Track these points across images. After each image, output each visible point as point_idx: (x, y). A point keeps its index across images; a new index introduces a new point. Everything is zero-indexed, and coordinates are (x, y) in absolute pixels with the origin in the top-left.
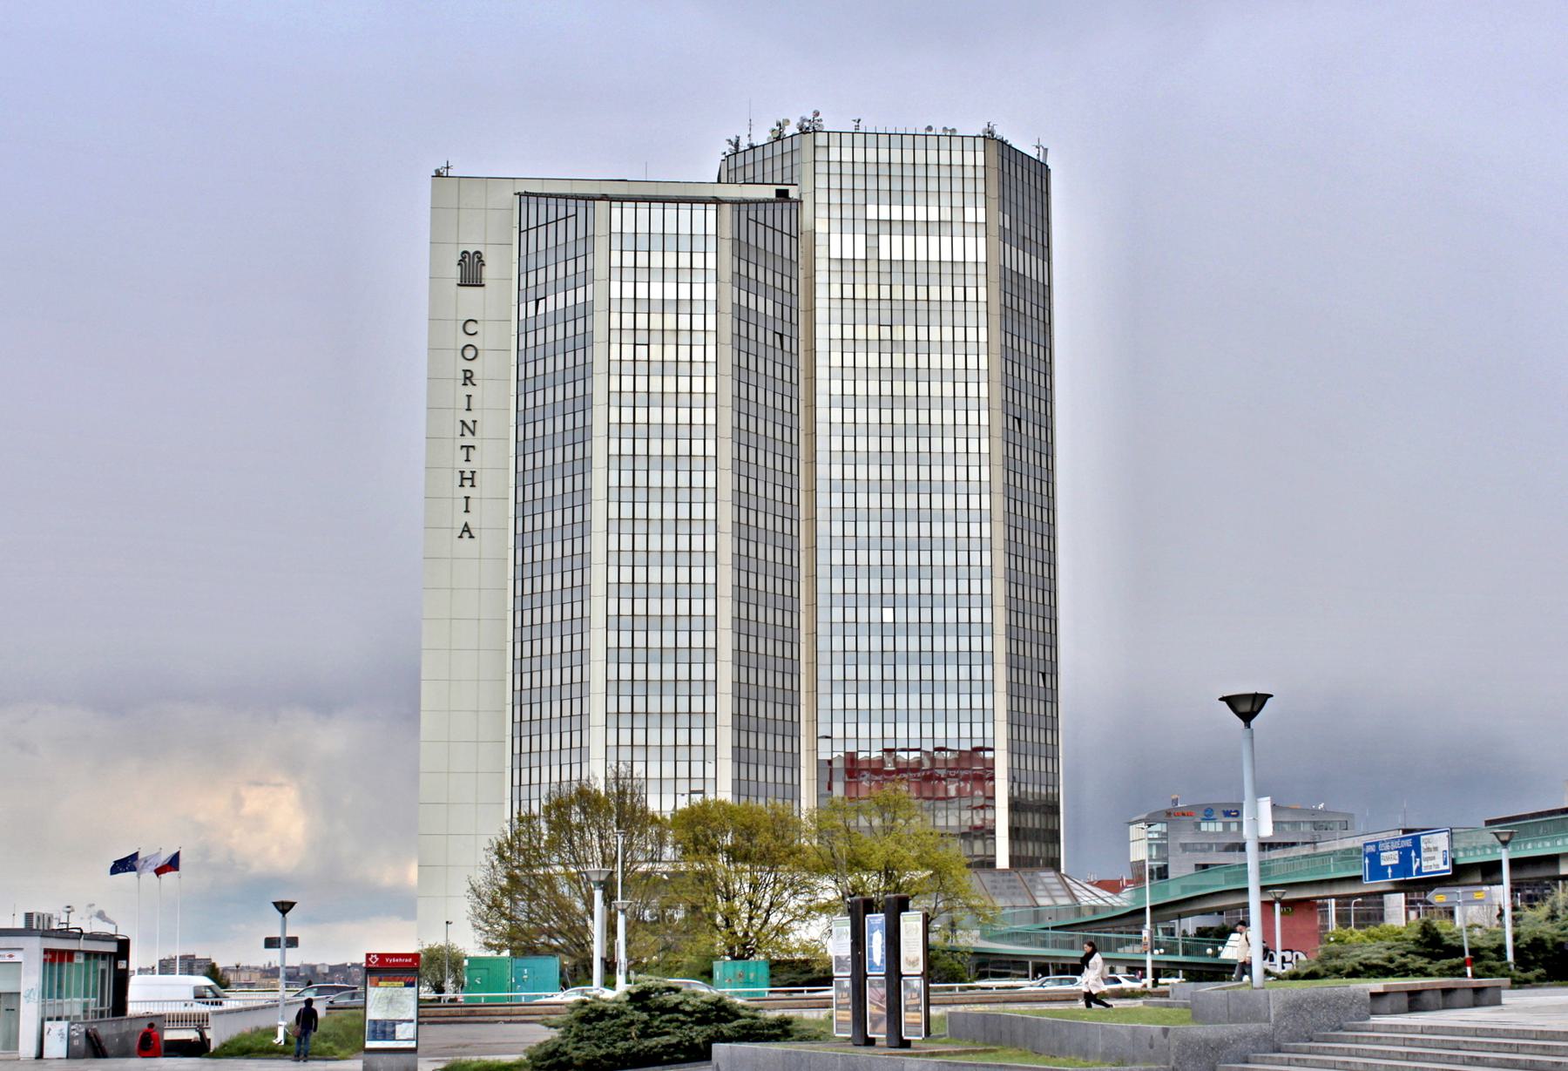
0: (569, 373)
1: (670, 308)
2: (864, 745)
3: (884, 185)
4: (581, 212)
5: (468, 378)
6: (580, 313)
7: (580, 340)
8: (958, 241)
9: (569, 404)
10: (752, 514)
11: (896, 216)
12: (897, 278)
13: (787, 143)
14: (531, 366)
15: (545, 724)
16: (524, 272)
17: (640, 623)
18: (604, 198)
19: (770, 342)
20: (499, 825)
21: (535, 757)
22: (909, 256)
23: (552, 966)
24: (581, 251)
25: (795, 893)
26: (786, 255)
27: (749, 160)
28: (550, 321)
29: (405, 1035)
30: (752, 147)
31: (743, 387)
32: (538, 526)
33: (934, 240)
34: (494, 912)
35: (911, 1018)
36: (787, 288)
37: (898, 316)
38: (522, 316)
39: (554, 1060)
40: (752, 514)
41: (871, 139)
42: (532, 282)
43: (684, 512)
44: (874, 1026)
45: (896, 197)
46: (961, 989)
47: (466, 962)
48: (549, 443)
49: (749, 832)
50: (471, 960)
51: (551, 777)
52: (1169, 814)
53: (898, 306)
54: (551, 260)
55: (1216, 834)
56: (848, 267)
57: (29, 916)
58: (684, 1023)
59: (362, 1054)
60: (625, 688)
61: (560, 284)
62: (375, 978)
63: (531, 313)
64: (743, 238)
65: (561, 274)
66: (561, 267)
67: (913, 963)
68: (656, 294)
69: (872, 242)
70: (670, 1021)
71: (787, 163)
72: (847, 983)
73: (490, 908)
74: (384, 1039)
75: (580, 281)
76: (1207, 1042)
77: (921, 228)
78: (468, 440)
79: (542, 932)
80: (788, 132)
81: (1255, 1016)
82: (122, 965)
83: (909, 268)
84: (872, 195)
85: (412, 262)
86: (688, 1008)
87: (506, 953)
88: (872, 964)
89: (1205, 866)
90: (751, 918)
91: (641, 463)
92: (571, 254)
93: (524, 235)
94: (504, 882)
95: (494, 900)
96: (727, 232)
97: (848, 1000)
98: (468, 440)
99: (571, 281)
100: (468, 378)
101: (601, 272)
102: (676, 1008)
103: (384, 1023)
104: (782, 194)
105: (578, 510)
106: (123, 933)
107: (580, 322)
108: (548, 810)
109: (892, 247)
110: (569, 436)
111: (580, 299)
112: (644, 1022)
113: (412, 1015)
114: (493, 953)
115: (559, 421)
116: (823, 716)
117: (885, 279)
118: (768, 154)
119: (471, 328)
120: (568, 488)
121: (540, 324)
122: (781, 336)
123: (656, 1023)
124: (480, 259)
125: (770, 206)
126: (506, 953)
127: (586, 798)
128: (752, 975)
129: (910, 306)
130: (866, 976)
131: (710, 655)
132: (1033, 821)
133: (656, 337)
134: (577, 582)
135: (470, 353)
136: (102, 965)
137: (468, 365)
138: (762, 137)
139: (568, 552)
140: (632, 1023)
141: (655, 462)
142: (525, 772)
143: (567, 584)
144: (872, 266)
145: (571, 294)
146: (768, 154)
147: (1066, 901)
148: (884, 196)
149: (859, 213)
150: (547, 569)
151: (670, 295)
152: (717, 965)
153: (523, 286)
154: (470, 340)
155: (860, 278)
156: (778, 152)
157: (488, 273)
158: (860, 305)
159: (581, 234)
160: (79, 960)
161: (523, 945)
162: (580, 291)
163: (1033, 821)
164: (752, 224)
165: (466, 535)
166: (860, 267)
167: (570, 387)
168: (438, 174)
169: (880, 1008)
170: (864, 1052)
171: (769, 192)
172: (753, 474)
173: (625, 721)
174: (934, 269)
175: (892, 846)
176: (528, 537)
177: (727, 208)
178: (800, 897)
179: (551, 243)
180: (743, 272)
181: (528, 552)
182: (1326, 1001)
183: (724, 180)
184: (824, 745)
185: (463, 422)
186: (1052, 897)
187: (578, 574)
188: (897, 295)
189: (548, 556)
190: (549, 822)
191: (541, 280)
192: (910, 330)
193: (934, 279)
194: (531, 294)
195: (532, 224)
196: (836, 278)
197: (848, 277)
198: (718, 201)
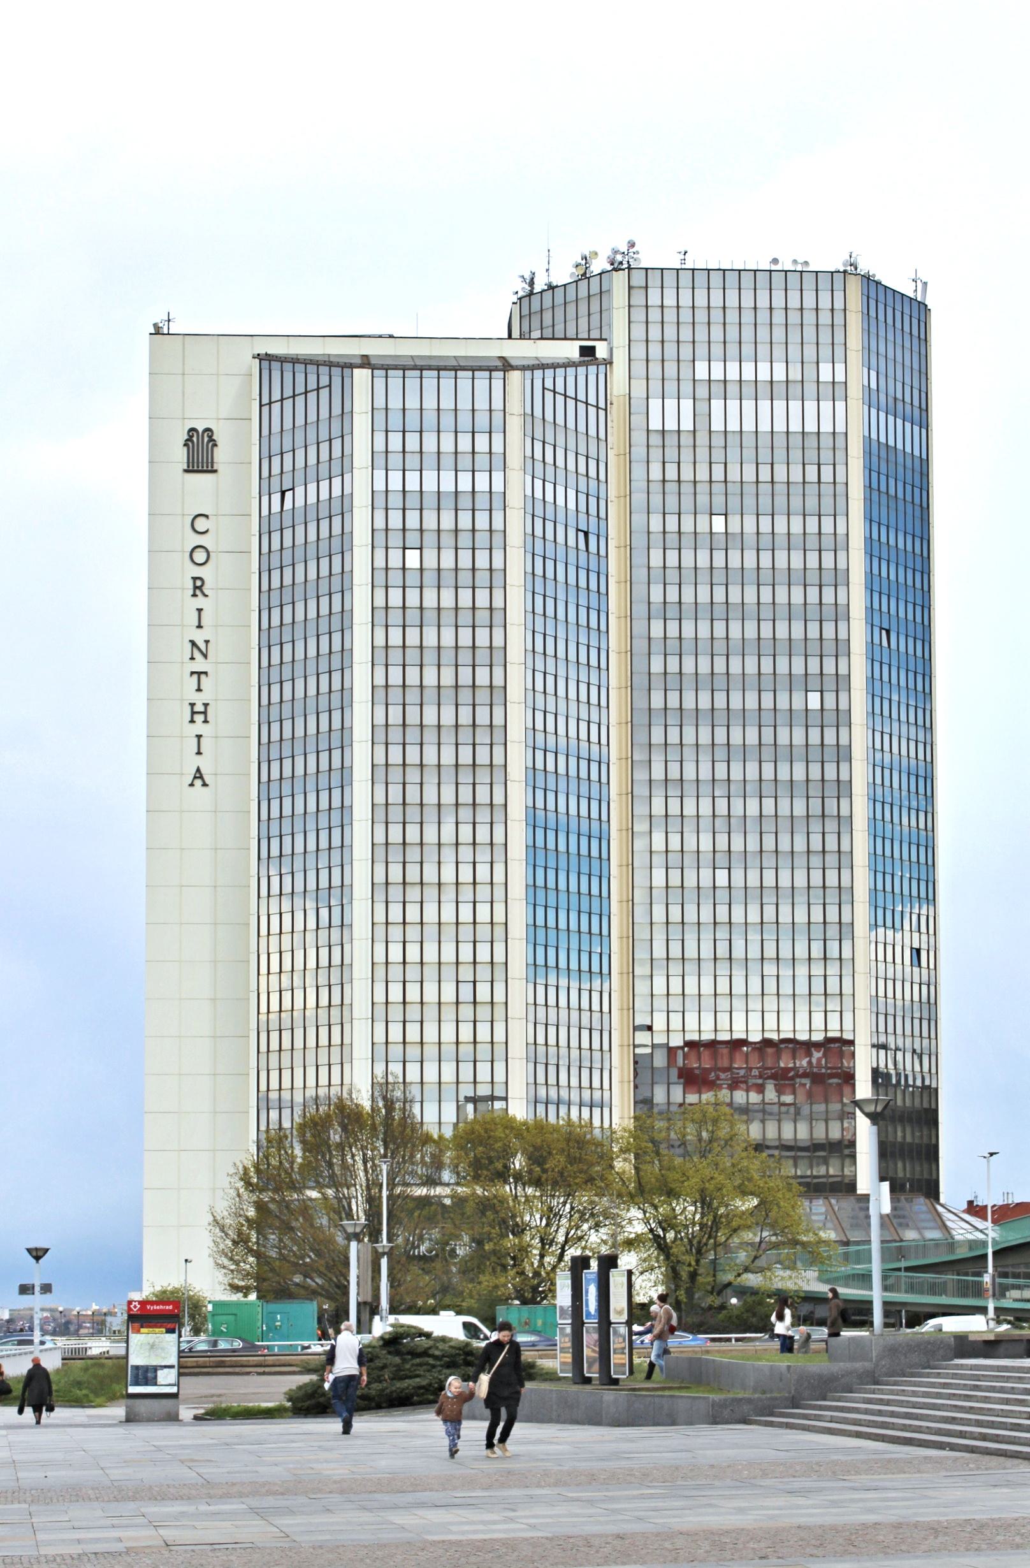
3: (717, 333)
4: (336, 381)
5: (198, 587)
6: (336, 509)
7: (336, 543)
8: (811, 406)
9: (324, 545)
10: (550, 757)
13: (595, 282)
14: (276, 574)
16: (266, 456)
19: (571, 542)
21: (286, 1056)
23: (308, 1311)
24: (336, 432)
25: (597, 1226)
26: (592, 431)
27: (548, 303)
28: (299, 519)
29: (167, 1380)
30: (551, 287)
31: (539, 600)
32: (287, 773)
33: (780, 405)
34: (241, 1248)
35: (618, 1359)
36: (592, 473)
37: (734, 502)
38: (265, 512)
39: (313, 1402)
41: (701, 278)
42: (276, 470)
44: (589, 1367)
46: (737, 1340)
47: (210, 1307)
48: (299, 595)
49: (537, 1157)
50: (216, 1304)
51: (305, 1085)
53: (734, 489)
56: (671, 441)
58: (434, 1366)
59: (124, 1401)
61: (312, 473)
62: (137, 1325)
63: (276, 508)
65: (312, 460)
67: (620, 1313)
68: (430, 486)
69: (702, 407)
70: (420, 1365)
71: (595, 307)
72: (568, 1330)
73: (235, 1243)
74: (146, 1384)
75: (336, 470)
76: (820, 1376)
79: (296, 1268)
80: (599, 265)
81: (865, 1357)
83: (749, 441)
86: (437, 1353)
87: (253, 1297)
88: (589, 1315)
90: (542, 1256)
92: (324, 436)
93: (265, 409)
94: (251, 1213)
95: (240, 1233)
97: (569, 1344)
98: (200, 664)
99: (324, 468)
100: (198, 587)
102: (425, 1353)
103: (146, 1369)
104: (588, 352)
108: (302, 1127)
109: (727, 415)
110: (324, 584)
111: (336, 492)
112: (397, 1365)
113: (173, 1360)
114: (238, 1297)
116: (641, 1004)
118: (571, 295)
119: (201, 524)
120: (324, 727)
121: (287, 522)
122: (586, 534)
123: (408, 1366)
124: (211, 439)
125: (571, 371)
126: (253, 1297)
127: (348, 1116)
128: (540, 1322)
129: (750, 489)
130: (584, 1323)
131: (499, 931)
132: (903, 1134)
134: (336, 803)
135: (200, 556)
138: (563, 275)
139: (324, 766)
140: (384, 1367)
143: (324, 805)
144: (703, 438)
145: (324, 485)
146: (571, 295)
147: (934, 1234)
149: (686, 373)
151: (448, 486)
153: (265, 474)
156: (583, 293)
158: (687, 489)
159: (336, 411)
161: (272, 1284)
162: (336, 482)
163: (903, 1134)
164: (549, 396)
165: (198, 782)
166: (686, 440)
167: (324, 601)
168: (157, 331)
169: (594, 1351)
171: (571, 350)
174: (780, 442)
175: (708, 1172)
177: (515, 376)
178: (602, 1230)
182: (918, 1345)
183: (516, 333)
184: (643, 1037)
185: (193, 643)
186: (918, 1229)
187: (336, 793)
188: (734, 475)
190: (303, 1142)
191: (288, 466)
195: (276, 396)
198: (506, 366)
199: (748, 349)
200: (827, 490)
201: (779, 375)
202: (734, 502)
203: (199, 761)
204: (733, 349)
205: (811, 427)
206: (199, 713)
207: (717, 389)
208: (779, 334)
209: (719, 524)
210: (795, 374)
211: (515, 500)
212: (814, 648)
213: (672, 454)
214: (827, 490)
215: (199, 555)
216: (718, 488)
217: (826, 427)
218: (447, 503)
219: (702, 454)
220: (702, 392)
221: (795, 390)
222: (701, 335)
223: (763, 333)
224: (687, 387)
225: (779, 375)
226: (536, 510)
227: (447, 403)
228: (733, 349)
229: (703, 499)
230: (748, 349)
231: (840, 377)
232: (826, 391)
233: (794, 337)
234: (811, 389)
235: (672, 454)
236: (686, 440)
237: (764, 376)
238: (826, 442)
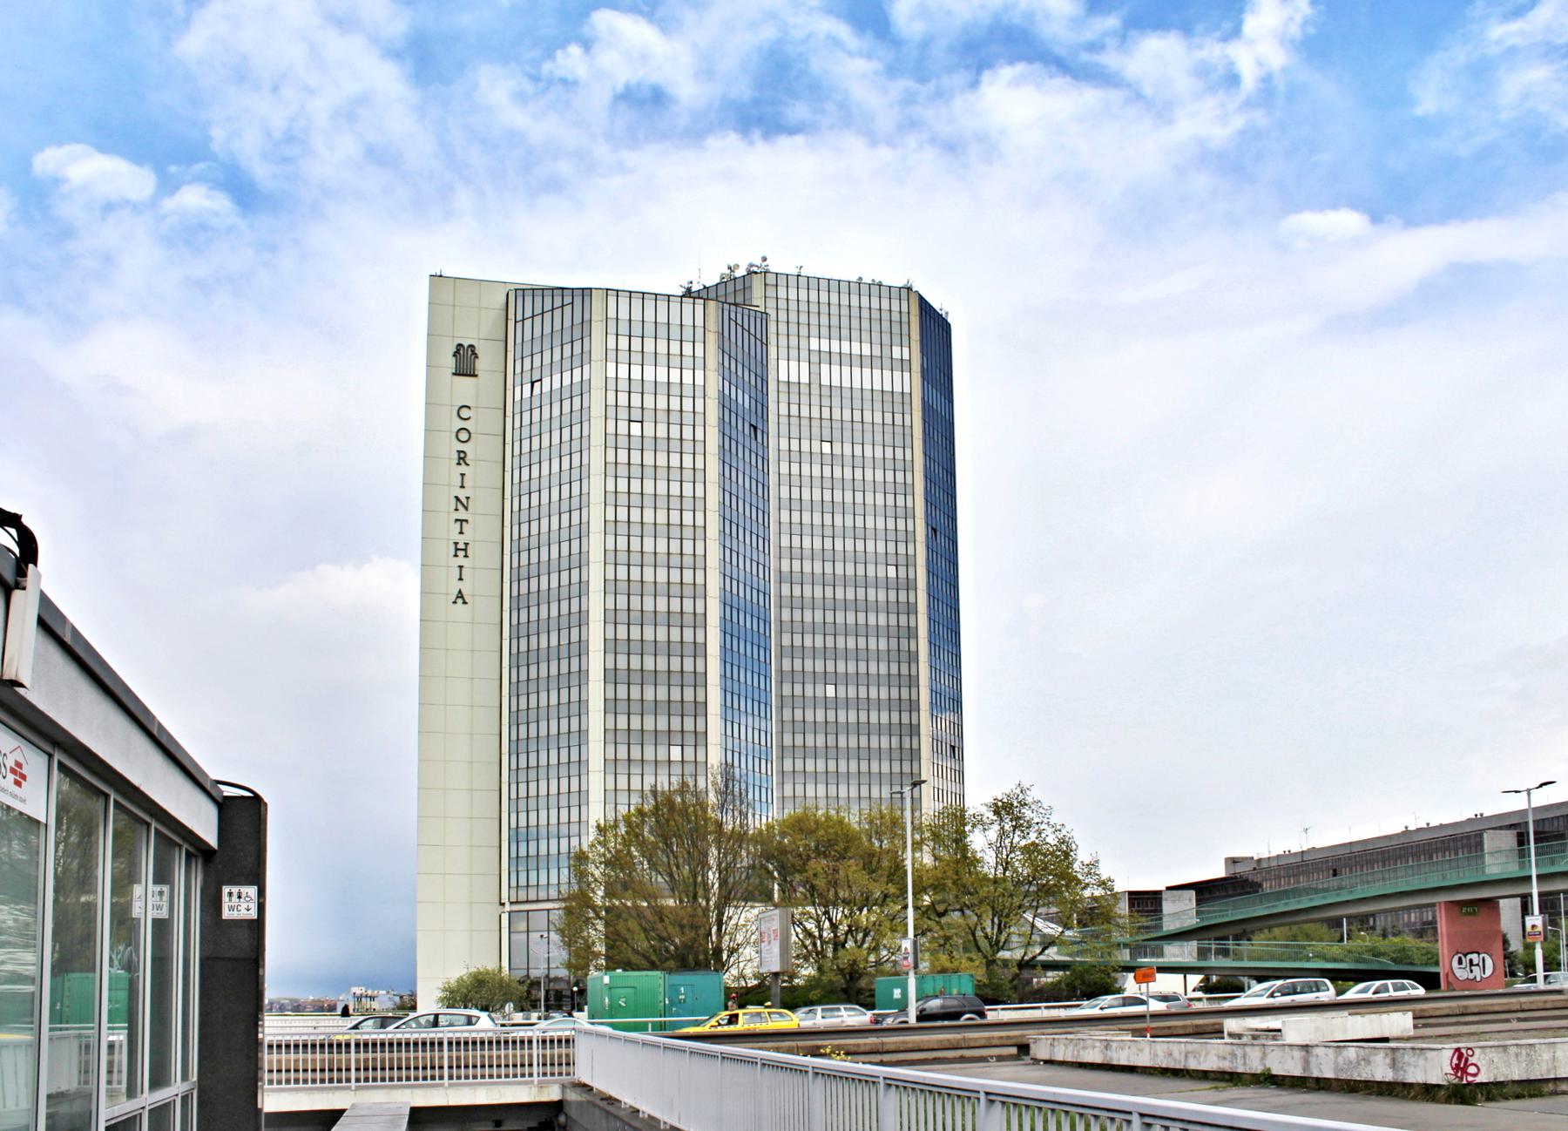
2: (822, 803)
3: (824, 320)
5: (462, 458)
12: (836, 401)
15: (543, 772)
17: (636, 678)
37: (837, 434)
56: (794, 389)
60: (622, 737)
69: (815, 368)
77: (856, 361)
80: (740, 273)
82: (237, 904)
83: (847, 394)
93: (519, 325)
96: (712, 325)
98: (462, 514)
100: (462, 458)
101: (597, 353)
109: (831, 375)
119: (465, 413)
124: (474, 353)
129: (847, 426)
137: (462, 447)
144: (815, 390)
145: (567, 375)
157: (481, 365)
158: (805, 422)
159: (578, 320)
162: (577, 372)
165: (460, 601)
166: (804, 390)
173: (622, 769)
174: (867, 396)
188: (836, 415)
195: (528, 314)
199: (845, 332)
200: (899, 430)
201: (866, 351)
202: (837, 434)
203: (461, 585)
204: (835, 332)
205: (887, 388)
206: (461, 550)
207: (825, 357)
208: (865, 324)
209: (826, 447)
210: (877, 352)
212: (635, 707)
213: (794, 398)
214: (899, 430)
216: (826, 424)
217: (898, 389)
218: (662, 390)
219: (815, 400)
220: (814, 358)
221: (877, 362)
222: (814, 320)
223: (855, 323)
224: (804, 354)
225: (866, 351)
227: (662, 318)
228: (835, 332)
229: (816, 431)
230: (845, 332)
231: (906, 357)
232: (897, 365)
233: (876, 327)
234: (887, 362)
235: (794, 398)
236: (804, 390)
237: (856, 351)
238: (898, 398)
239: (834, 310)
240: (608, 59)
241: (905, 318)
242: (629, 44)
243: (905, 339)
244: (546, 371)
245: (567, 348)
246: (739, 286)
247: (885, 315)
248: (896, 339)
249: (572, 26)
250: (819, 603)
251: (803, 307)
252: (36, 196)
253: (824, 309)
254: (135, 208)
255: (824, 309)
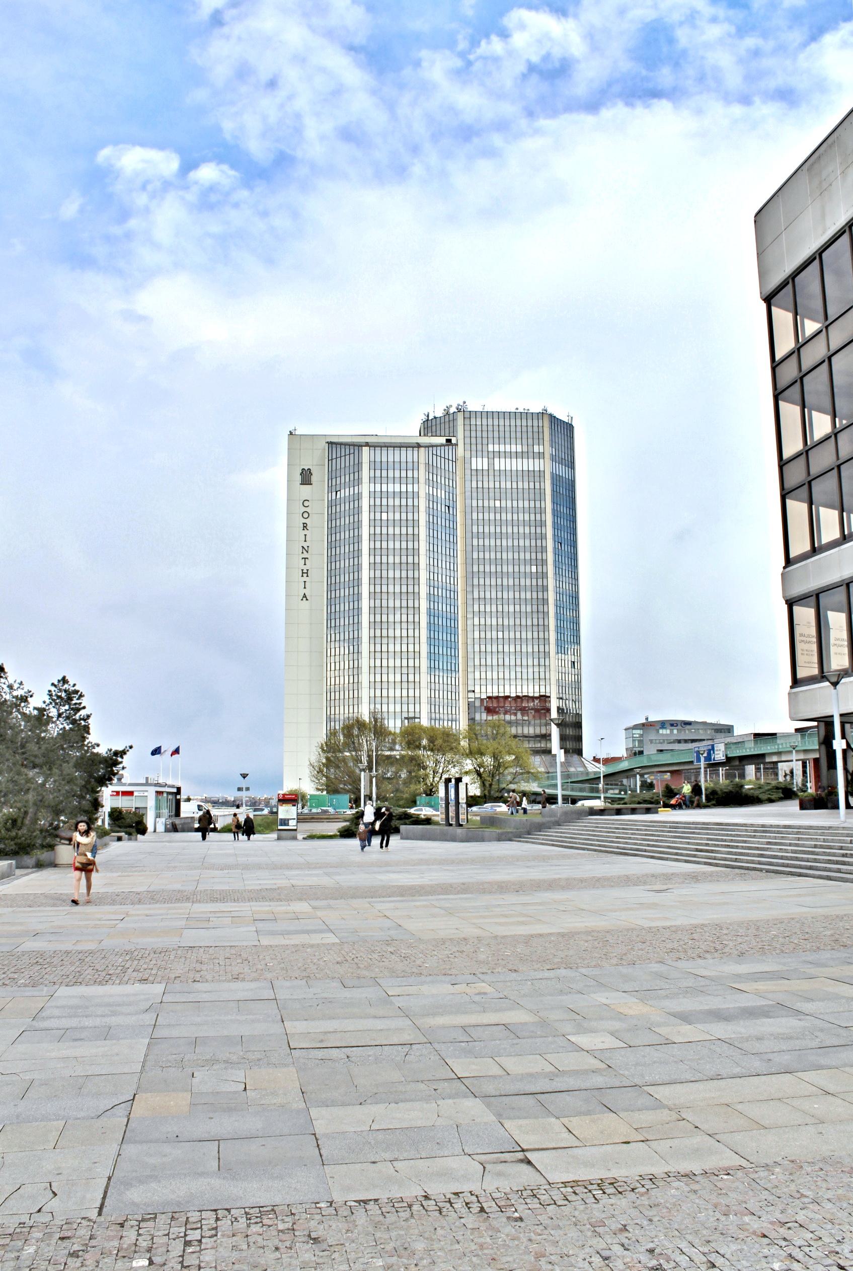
0: (351, 526)
1: (397, 496)
5: (305, 526)
6: (356, 498)
11: (502, 449)
12: (503, 478)
14: (334, 522)
18: (367, 444)
20: (322, 738)
22: (508, 468)
27: (434, 423)
29: (292, 824)
30: (435, 418)
32: (338, 595)
35: (462, 817)
40: (436, 590)
42: (334, 483)
43: (404, 589)
45: (502, 440)
49: (432, 740)
50: (311, 796)
51: (344, 713)
52: (643, 725)
54: (343, 473)
55: (667, 735)
56: (480, 473)
57: (147, 778)
63: (334, 497)
64: (431, 463)
66: (347, 477)
68: (391, 489)
78: (305, 555)
80: (452, 410)
81: (555, 816)
82: (178, 797)
83: (508, 474)
84: (490, 440)
85: (277, 476)
89: (661, 751)
91: (384, 567)
94: (324, 761)
98: (305, 555)
100: (305, 526)
103: (285, 820)
104: (449, 441)
105: (356, 559)
106: (178, 784)
107: (356, 502)
108: (343, 729)
109: (500, 464)
111: (356, 492)
113: (295, 817)
114: (319, 793)
115: (347, 533)
116: (471, 682)
117: (497, 478)
118: (443, 421)
119: (306, 504)
126: (325, 793)
127: (361, 725)
129: (509, 491)
131: (417, 655)
132: (570, 732)
133: (391, 509)
135: (306, 515)
136: (170, 797)
138: (439, 413)
141: (391, 566)
142: (333, 709)
145: (352, 489)
147: (581, 769)
148: (496, 440)
150: (342, 615)
152: (418, 798)
154: (306, 509)
155: (486, 478)
159: (356, 462)
160: (165, 795)
161: (332, 789)
163: (570, 732)
164: (435, 457)
166: (485, 473)
167: (352, 532)
168: (291, 433)
170: (451, 828)
171: (443, 440)
172: (436, 571)
173: (378, 626)
176: (333, 600)
177: (422, 449)
179: (343, 466)
180: (431, 478)
181: (333, 607)
184: (471, 695)
188: (503, 486)
189: (342, 609)
192: (509, 503)
193: (520, 478)
194: (333, 489)
195: (334, 457)
196: (474, 478)
197: (480, 478)
201: (519, 450)
208: (519, 435)
211: (422, 494)
215: (306, 515)
225: (519, 450)
226: (430, 498)
233: (525, 436)
236: (485, 473)
239: (502, 429)
240: (519, 40)
241: (541, 430)
242: (534, 31)
243: (541, 441)
244: (343, 486)
245: (352, 475)
246: (451, 418)
247: (530, 429)
248: (536, 441)
249: (491, 25)
250: (505, 589)
251: (485, 428)
252: (98, 182)
253: (496, 428)
254: (167, 185)
255: (496, 428)
